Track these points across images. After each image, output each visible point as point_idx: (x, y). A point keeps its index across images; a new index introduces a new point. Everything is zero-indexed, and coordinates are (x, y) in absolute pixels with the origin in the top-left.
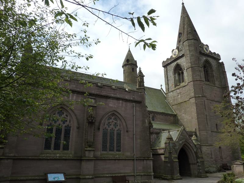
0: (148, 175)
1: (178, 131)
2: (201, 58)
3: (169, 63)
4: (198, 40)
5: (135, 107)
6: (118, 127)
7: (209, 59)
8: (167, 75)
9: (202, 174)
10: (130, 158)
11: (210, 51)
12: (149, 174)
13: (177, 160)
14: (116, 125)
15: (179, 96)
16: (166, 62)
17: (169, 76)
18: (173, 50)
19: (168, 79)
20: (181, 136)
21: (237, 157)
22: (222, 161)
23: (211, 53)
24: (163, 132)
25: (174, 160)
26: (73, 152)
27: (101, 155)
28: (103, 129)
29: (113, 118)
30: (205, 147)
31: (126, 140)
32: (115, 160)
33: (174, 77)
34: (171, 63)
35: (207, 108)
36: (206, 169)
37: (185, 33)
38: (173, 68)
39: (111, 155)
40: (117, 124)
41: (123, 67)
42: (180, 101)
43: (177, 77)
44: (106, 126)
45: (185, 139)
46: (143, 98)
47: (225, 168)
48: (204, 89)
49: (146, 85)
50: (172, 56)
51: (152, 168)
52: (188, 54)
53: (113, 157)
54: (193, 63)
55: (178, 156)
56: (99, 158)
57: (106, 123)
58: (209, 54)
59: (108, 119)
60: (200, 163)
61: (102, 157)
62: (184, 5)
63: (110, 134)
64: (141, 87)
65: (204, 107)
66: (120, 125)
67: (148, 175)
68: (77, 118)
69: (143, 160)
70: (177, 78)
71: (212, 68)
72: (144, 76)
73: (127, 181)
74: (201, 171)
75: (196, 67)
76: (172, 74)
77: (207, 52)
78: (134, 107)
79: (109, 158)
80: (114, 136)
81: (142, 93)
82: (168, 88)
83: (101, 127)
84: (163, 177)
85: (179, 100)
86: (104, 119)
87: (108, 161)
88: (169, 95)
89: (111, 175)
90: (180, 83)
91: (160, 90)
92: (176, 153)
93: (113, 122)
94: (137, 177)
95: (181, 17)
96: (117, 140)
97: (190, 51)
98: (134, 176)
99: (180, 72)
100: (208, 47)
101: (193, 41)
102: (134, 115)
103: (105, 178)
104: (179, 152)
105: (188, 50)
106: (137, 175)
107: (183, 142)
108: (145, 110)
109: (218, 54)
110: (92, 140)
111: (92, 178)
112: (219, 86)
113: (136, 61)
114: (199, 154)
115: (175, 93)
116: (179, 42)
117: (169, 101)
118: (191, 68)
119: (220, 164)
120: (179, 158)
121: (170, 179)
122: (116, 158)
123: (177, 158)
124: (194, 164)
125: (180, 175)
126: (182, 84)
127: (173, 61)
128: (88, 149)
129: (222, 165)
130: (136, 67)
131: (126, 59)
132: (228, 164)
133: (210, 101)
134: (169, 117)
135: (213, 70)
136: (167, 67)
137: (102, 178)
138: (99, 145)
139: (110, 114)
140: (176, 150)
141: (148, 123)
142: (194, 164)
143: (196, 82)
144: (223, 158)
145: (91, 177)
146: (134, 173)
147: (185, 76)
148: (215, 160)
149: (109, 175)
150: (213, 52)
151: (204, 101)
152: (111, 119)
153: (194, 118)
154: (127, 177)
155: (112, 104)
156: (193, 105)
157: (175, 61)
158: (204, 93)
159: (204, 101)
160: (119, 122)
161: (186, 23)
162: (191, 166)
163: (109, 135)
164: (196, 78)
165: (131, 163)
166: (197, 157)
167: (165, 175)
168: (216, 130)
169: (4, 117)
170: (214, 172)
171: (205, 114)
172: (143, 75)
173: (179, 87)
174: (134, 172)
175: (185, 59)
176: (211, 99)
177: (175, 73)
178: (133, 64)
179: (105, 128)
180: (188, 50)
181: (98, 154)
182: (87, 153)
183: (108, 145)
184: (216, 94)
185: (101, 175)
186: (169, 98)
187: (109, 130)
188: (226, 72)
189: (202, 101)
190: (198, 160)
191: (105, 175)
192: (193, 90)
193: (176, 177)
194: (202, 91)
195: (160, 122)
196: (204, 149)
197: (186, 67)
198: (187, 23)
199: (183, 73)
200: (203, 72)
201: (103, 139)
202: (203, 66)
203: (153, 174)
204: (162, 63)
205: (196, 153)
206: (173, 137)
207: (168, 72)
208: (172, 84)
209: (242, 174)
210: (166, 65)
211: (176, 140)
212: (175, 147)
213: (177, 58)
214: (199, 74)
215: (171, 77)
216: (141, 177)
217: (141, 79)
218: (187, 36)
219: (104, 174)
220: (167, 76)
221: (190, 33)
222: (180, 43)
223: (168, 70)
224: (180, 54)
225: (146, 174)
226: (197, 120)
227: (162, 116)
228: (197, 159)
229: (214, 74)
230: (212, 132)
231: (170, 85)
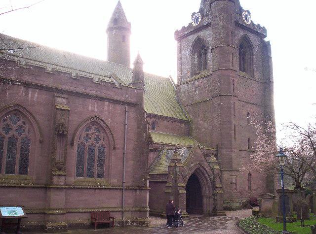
6: (101, 142)
14: (97, 138)
18: (194, 14)
23: (253, 25)
26: (34, 177)
29: (94, 127)
31: (113, 162)
44: (83, 140)
46: (141, 99)
48: (235, 83)
51: (148, 201)
55: (187, 186)
57: (84, 135)
65: (233, 112)
68: (39, 127)
69: (136, 190)
71: (252, 50)
76: (188, 53)
81: (140, 91)
86: (80, 130)
87: (85, 191)
89: (89, 210)
93: (93, 133)
98: (122, 211)
110: (63, 161)
111: (63, 214)
114: (216, 183)
120: (187, 188)
126: (204, 73)
128: (57, 173)
133: (243, 103)
137: (76, 214)
138: (73, 169)
142: (209, 197)
145: (61, 212)
149: (86, 210)
150: (256, 23)
154: (111, 213)
155: (93, 107)
158: (235, 91)
162: (205, 200)
163: (19, 145)
165: (118, 194)
166: (214, 187)
168: (247, 148)
173: (198, 76)
175: (211, 32)
177: (193, 53)
181: (72, 179)
182: (55, 179)
191: (80, 211)
196: (226, 176)
199: (206, 54)
202: (238, 46)
203: (148, 209)
205: (213, 182)
206: (217, 218)
210: (182, 36)
216: (131, 214)
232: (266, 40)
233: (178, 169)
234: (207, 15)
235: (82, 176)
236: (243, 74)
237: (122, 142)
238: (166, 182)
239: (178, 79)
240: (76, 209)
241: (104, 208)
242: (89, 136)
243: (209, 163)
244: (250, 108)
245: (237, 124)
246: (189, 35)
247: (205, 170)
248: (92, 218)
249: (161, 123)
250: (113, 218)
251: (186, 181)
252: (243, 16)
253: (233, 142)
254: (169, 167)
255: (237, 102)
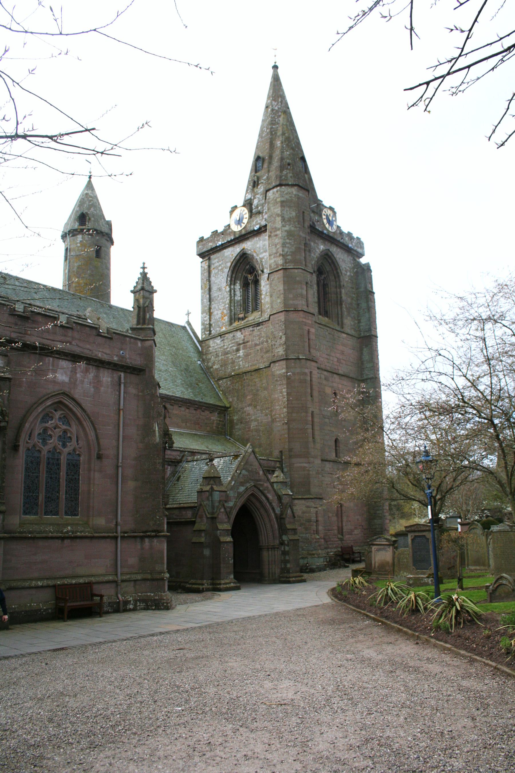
0: (153, 580)
1: (236, 457)
2: (312, 244)
3: (217, 247)
4: (308, 191)
5: (125, 384)
6: (71, 446)
7: (334, 250)
8: (210, 281)
9: (291, 575)
10: (106, 535)
11: (338, 227)
12: (158, 577)
13: (229, 539)
14: (65, 438)
15: (241, 353)
16: (211, 241)
17: (214, 288)
19: (210, 295)
20: (244, 472)
21: (378, 530)
22: (341, 540)
23: (341, 233)
24: (190, 458)
25: (222, 539)
27: (22, 524)
28: (28, 449)
29: (58, 415)
30: (303, 502)
32: (63, 539)
33: (230, 291)
34: (224, 247)
35: (316, 394)
36: (302, 562)
37: (276, 163)
38: (229, 264)
39: (51, 524)
40: (69, 435)
41: (64, 237)
42: (243, 365)
43: (238, 293)
44: (36, 439)
45: (252, 480)
47: (347, 557)
48: (312, 337)
49: (156, 315)
50: (229, 225)
52: (276, 229)
53: (58, 532)
54: (289, 257)
56: (17, 535)
58: (335, 237)
59: (43, 418)
60: (288, 545)
61: (25, 532)
62: (279, 71)
63: (48, 463)
64: (144, 323)
65: (309, 390)
66: (77, 437)
67: (153, 580)
69: (142, 538)
70: (238, 297)
71: (339, 277)
72: (156, 291)
73: (97, 596)
74: (288, 566)
75: (296, 271)
77: (330, 229)
78: (122, 386)
79: (44, 535)
80: (59, 469)
81: (148, 343)
82: (210, 325)
83: (21, 443)
84: (188, 586)
85: (239, 365)
86: (31, 419)
87: (41, 543)
88: (210, 347)
89: (51, 583)
90: (246, 310)
91: (184, 328)
92: (229, 518)
94: (124, 584)
95: (267, 107)
96: (69, 481)
97: (283, 220)
98: (115, 582)
99: (250, 277)
100: (334, 213)
101: (294, 190)
102: (121, 407)
103: (33, 591)
104: (235, 519)
105: (278, 215)
106: (123, 581)
107: (247, 489)
108: (153, 396)
109: (358, 238)
112: (353, 332)
113: (109, 224)
115: (228, 343)
116: (254, 186)
117: (210, 364)
118: (281, 272)
119: (336, 547)
120: (234, 533)
121: (208, 590)
122: (66, 535)
123: (230, 533)
124: (273, 548)
125: (235, 578)
126: (253, 317)
127: (231, 241)
129: (338, 551)
130: (108, 244)
131: (77, 211)
132: (354, 548)
133: (325, 373)
134: (207, 413)
135: (342, 284)
136: (209, 259)
139: (49, 403)
140: (228, 510)
141: (160, 435)
142: (273, 548)
143: (293, 316)
144: (344, 531)
146: (117, 575)
147: (264, 293)
148: (324, 539)
149: (45, 583)
151: (311, 372)
152: (52, 418)
153: (279, 421)
154: (95, 587)
156: (279, 383)
157: (236, 243)
158: (312, 351)
159: (311, 372)
160: (74, 428)
161: (279, 133)
162: (265, 555)
163: (43, 467)
164: (296, 302)
165: (107, 547)
166: (283, 530)
167: (193, 581)
168: (333, 456)
169: (216, 427)
170: (321, 569)
171: (311, 410)
172: (152, 287)
174: (116, 571)
175: (267, 243)
176: (329, 369)
177: (232, 282)
178: (99, 233)
179: (34, 446)
180: (278, 215)
183: (41, 497)
184: (342, 353)
185: (19, 584)
186: (209, 356)
187: (46, 452)
188: (374, 293)
189: (305, 374)
190: (285, 538)
191: (34, 583)
192: (284, 338)
193: (224, 584)
194: (307, 344)
195: (179, 427)
196: (300, 507)
197: (270, 266)
198: (283, 134)
199: (256, 282)
200: (315, 286)
201: (27, 477)
202: (316, 270)
203: (167, 575)
204: (198, 242)
205: (280, 519)
207: (213, 272)
208: (222, 313)
209: (387, 568)
211: (230, 482)
212: (226, 501)
213: (245, 235)
214: (304, 292)
215: (220, 289)
216: (134, 586)
217: (147, 298)
218: (278, 173)
219: (31, 580)
220: (210, 286)
221: (289, 164)
222: (256, 190)
223: (212, 267)
224: (254, 223)
225: (149, 577)
226: (286, 427)
227: (187, 410)
228: (281, 536)
229: (344, 297)
230: (322, 460)
231: (217, 314)
232: (363, 261)
233: (217, 496)
234: (259, 213)
235: (57, 514)
236: (324, 320)
237: (114, 443)
238: (193, 523)
239: (204, 330)
240: (25, 580)
241: (82, 577)
242: (50, 432)
243: (272, 484)
244: (337, 382)
245: (316, 411)
246: (225, 248)
247: (267, 498)
248: (57, 599)
249: (175, 412)
250: (101, 596)
251: (233, 517)
252: (324, 217)
253: (311, 445)
254: (200, 492)
255: (315, 372)
